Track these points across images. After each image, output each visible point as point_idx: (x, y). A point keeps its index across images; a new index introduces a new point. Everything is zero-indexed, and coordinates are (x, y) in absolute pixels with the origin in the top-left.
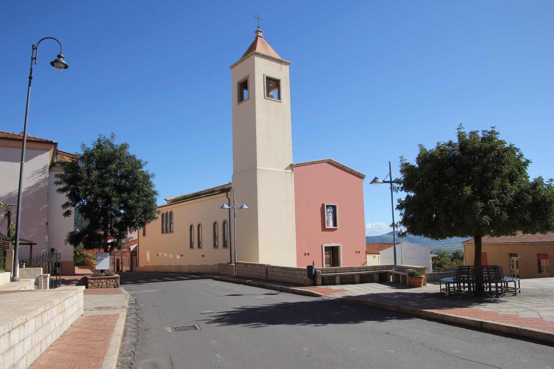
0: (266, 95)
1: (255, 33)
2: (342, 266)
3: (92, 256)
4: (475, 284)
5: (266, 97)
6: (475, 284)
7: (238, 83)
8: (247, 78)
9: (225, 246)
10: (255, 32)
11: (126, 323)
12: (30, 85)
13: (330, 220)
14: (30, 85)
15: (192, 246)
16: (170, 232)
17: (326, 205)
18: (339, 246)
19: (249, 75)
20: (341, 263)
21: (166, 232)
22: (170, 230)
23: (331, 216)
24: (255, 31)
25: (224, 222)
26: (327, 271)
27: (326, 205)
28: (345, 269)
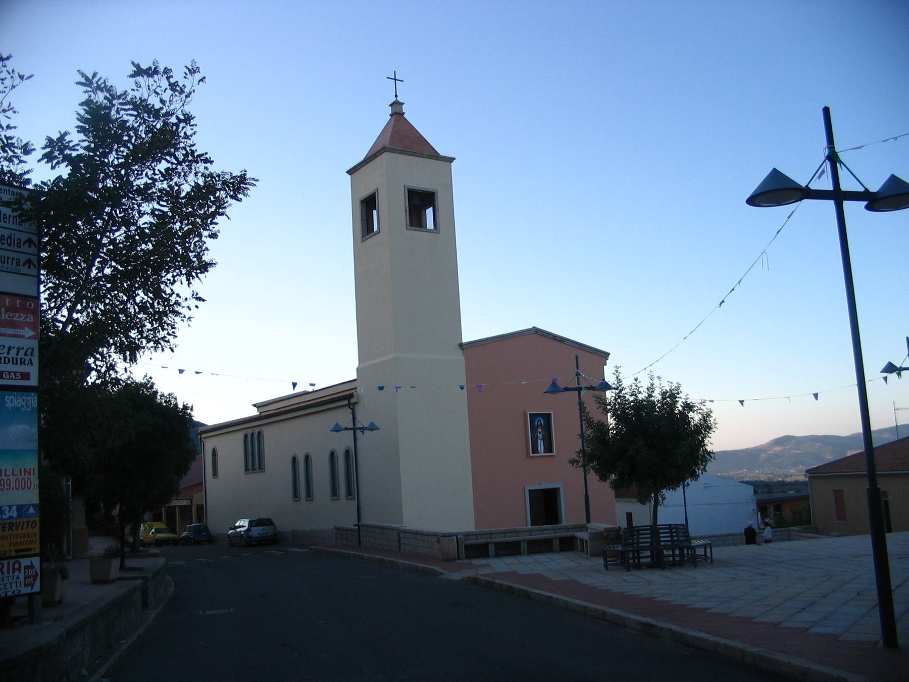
0: (408, 224)
1: (390, 108)
2: (564, 524)
3: (166, 106)
4: (42, 199)
5: (409, 228)
6: (42, 199)
7: (825, 107)
8: (375, 193)
9: (349, 493)
10: (390, 105)
11: (155, 199)
12: (793, 212)
13: (539, 441)
14: (793, 212)
15: (296, 494)
16: (260, 468)
17: (530, 414)
18: (559, 488)
19: (377, 189)
20: (564, 518)
21: (254, 469)
22: (260, 465)
23: (540, 433)
24: (390, 103)
25: (347, 452)
26: (530, 532)
27: (530, 414)
28: (567, 528)
